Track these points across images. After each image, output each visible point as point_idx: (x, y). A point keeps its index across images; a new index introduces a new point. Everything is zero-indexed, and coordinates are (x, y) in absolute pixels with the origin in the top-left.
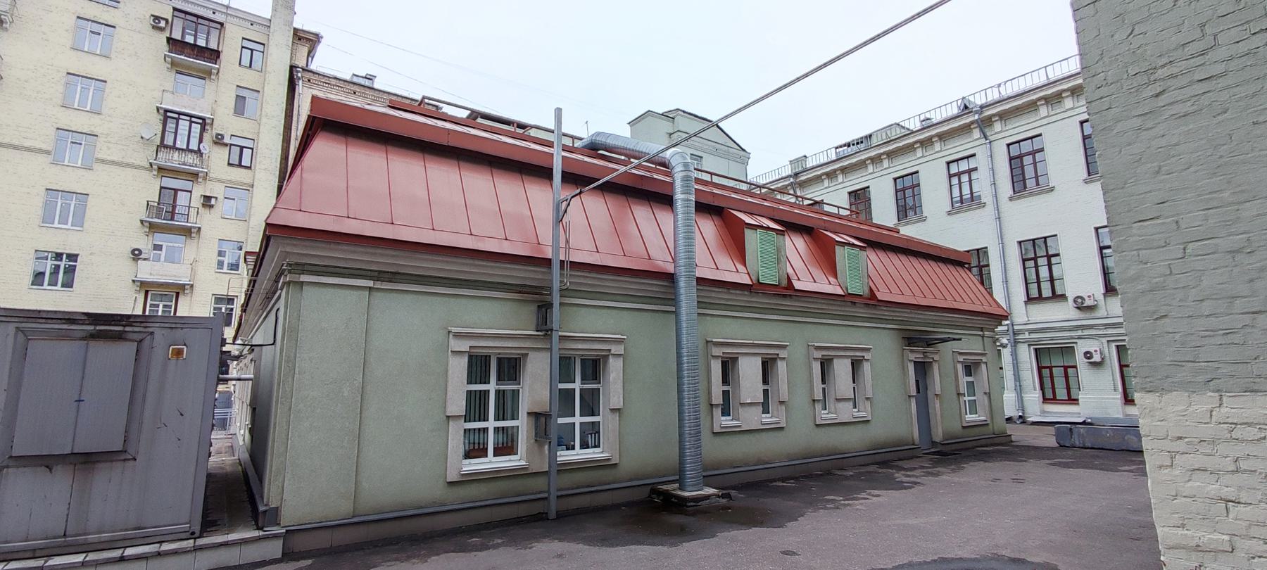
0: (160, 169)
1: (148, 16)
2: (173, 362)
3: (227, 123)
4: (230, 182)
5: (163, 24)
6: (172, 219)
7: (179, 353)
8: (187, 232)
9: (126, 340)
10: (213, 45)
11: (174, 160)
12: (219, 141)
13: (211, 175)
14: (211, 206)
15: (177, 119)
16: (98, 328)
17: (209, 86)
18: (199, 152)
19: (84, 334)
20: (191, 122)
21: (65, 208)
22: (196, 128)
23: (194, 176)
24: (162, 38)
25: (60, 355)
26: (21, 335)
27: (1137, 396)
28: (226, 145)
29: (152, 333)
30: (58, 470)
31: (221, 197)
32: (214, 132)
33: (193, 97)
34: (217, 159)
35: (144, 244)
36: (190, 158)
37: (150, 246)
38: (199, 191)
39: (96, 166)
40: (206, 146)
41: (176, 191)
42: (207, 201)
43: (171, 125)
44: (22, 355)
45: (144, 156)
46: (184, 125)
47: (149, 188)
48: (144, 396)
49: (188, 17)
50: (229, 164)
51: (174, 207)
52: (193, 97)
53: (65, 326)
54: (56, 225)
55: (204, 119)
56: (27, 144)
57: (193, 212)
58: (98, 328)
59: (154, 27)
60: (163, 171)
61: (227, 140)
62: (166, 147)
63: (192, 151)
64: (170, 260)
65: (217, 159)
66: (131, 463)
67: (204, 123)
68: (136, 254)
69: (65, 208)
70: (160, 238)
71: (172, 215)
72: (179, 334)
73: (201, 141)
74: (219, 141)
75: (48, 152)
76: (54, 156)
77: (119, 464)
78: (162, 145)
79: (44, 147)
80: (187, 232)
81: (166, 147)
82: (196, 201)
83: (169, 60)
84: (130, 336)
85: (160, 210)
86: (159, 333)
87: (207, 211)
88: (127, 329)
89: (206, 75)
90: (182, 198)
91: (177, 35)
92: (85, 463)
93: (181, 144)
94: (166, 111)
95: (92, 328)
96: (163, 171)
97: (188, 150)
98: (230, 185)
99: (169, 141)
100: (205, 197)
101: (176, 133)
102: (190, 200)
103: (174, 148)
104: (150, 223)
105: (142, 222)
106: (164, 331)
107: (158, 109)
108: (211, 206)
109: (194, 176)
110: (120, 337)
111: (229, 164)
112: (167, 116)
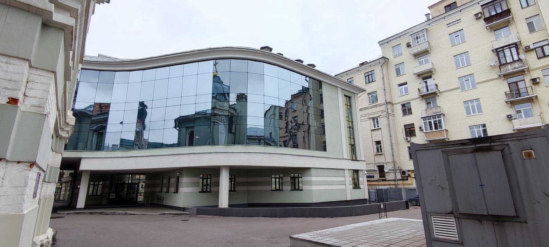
0: (505, 76)
1: (473, 16)
2: (528, 160)
3: (529, 39)
4: (543, 67)
5: (480, 15)
6: (520, 96)
7: (529, 155)
8: (531, 100)
9: (494, 150)
10: (505, 8)
11: (510, 69)
12: (528, 50)
13: (531, 68)
14: (538, 83)
15: (503, 50)
16: (478, 145)
17: (512, 28)
18: (520, 60)
19: (472, 150)
20: (510, 48)
21: (473, 107)
22: (514, 50)
23: (522, 72)
24: (482, 22)
25: (463, 161)
26: (444, 153)
27: (376, 169)
28: (533, 50)
29: (507, 145)
30: (484, 222)
31: (541, 77)
32: (523, 47)
33: (506, 37)
34: (531, 59)
35: (512, 112)
36: (516, 65)
37: (515, 112)
38: (528, 79)
39: (477, 86)
40: (522, 57)
41: (516, 83)
42: (535, 81)
43: (501, 55)
44: (447, 164)
45: (494, 74)
46: (507, 52)
47: (503, 87)
48: (518, 183)
49: (489, 5)
50: (539, 58)
51: (519, 90)
52: (506, 37)
53: (461, 147)
54: (472, 114)
55: (515, 44)
56: (451, 88)
57: (529, 90)
58: (478, 145)
59: (477, 19)
60: (506, 76)
61: (532, 47)
62: (503, 65)
63: (516, 61)
64: (527, 115)
65: (531, 59)
66: (524, 225)
67: (516, 45)
68: (510, 118)
69: (473, 107)
70: (518, 107)
71: (519, 94)
72: (525, 143)
73: (518, 54)
74: (528, 50)
75: (459, 88)
76: (463, 88)
77: (518, 225)
78: (501, 65)
79: (456, 87)
80: (531, 100)
81: (503, 65)
82: (529, 84)
83: (491, 28)
84: (496, 148)
85: (512, 94)
86: (511, 144)
87: (537, 86)
88: (493, 144)
89: (507, 24)
90: (521, 85)
91: (487, 15)
92: (497, 221)
93: (509, 60)
94: (496, 49)
95: (474, 146)
96: (506, 76)
97: (514, 61)
98: (543, 69)
99: (503, 62)
100: (532, 79)
101: (505, 57)
102: (525, 83)
103: (507, 64)
104: (510, 101)
105: (506, 102)
106: (514, 143)
107: (492, 51)
108: (538, 83)
109: (522, 72)
110: (489, 149)
111: (539, 58)
112: (498, 51)
